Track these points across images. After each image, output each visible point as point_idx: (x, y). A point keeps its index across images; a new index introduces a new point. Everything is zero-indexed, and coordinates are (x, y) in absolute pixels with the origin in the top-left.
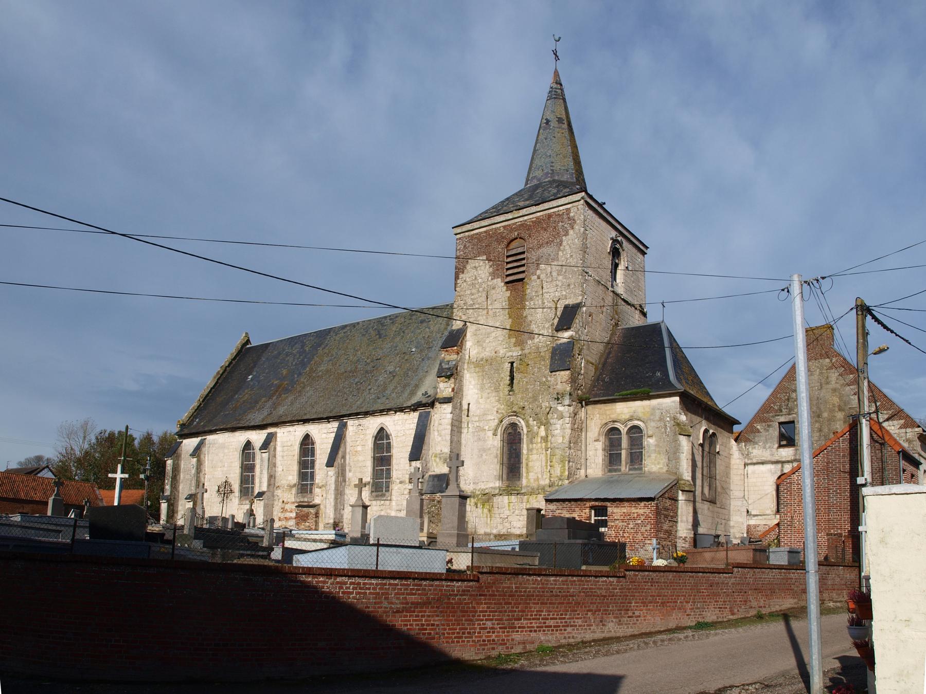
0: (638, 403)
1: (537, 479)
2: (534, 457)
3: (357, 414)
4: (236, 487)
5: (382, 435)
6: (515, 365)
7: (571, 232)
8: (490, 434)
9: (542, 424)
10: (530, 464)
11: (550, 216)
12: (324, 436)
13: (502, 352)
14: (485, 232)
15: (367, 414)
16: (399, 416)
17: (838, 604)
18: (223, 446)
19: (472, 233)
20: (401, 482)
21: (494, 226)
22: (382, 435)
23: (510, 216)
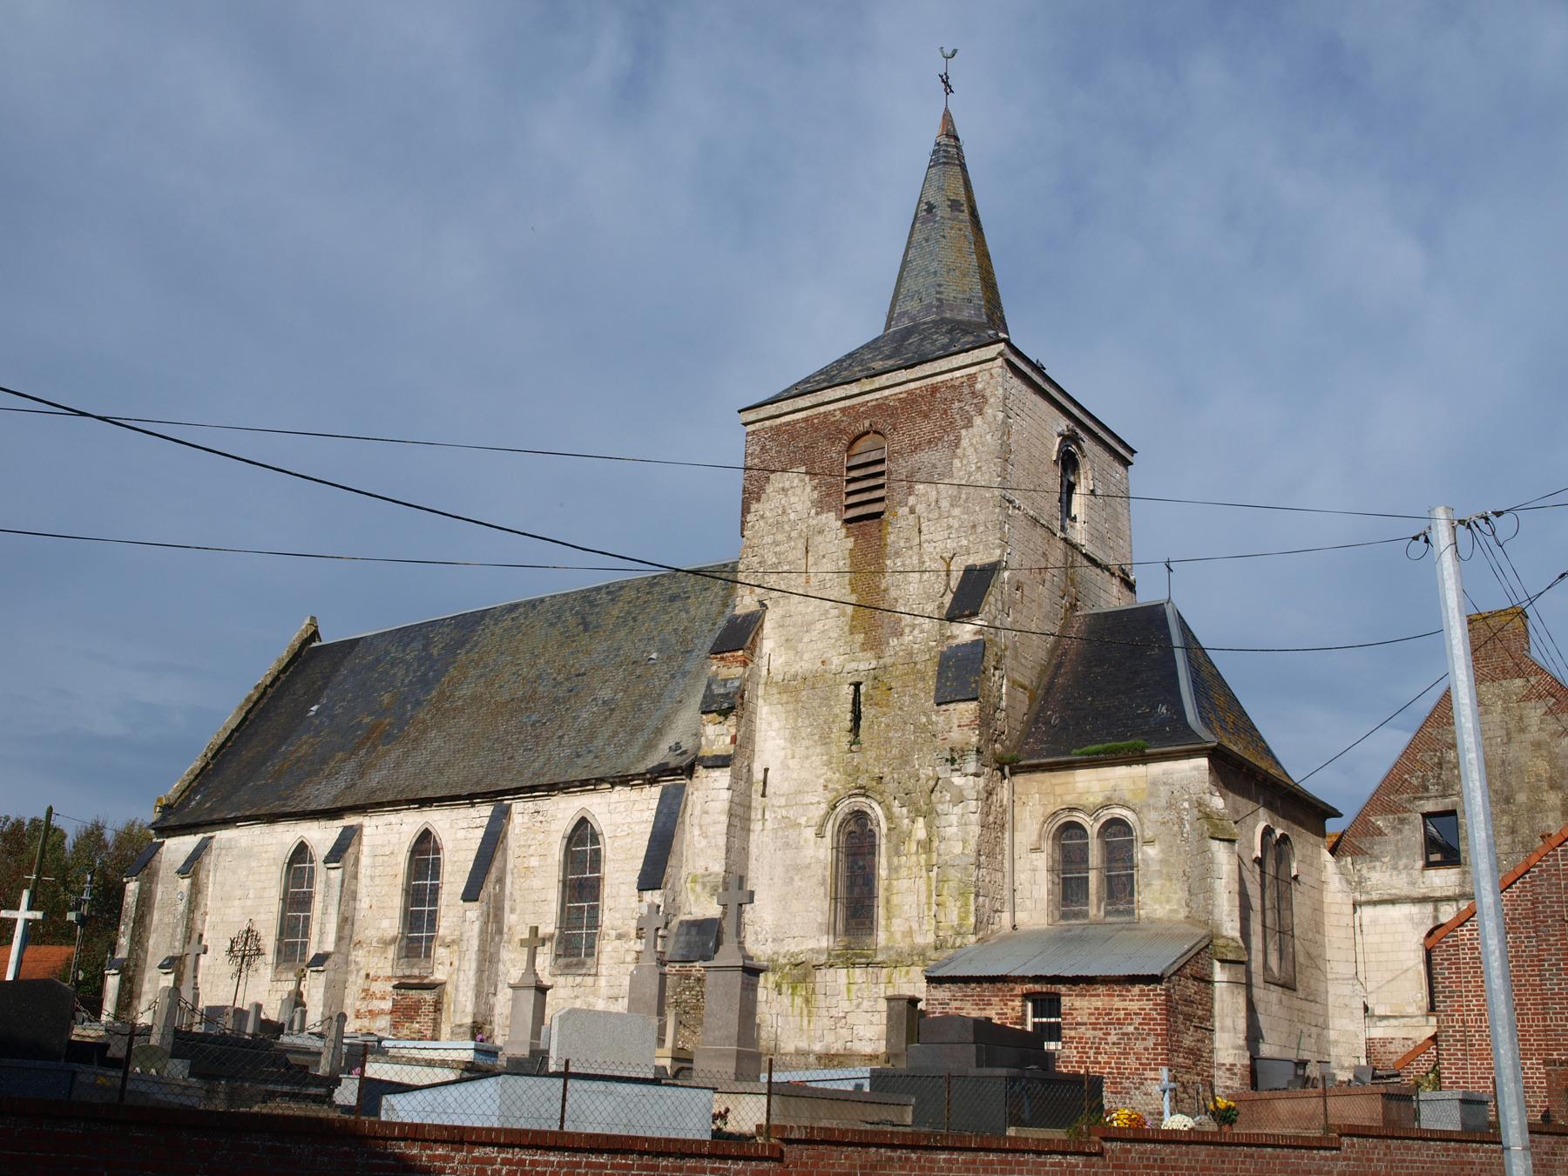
0: (1122, 771)
1: (910, 933)
2: (902, 884)
4: (269, 942)
6: (863, 689)
7: (978, 420)
8: (810, 833)
9: (918, 813)
10: (895, 900)
11: (934, 389)
12: (461, 834)
13: (836, 662)
14: (805, 420)
15: (553, 788)
16: (621, 794)
20: (619, 937)
23: (854, 389)
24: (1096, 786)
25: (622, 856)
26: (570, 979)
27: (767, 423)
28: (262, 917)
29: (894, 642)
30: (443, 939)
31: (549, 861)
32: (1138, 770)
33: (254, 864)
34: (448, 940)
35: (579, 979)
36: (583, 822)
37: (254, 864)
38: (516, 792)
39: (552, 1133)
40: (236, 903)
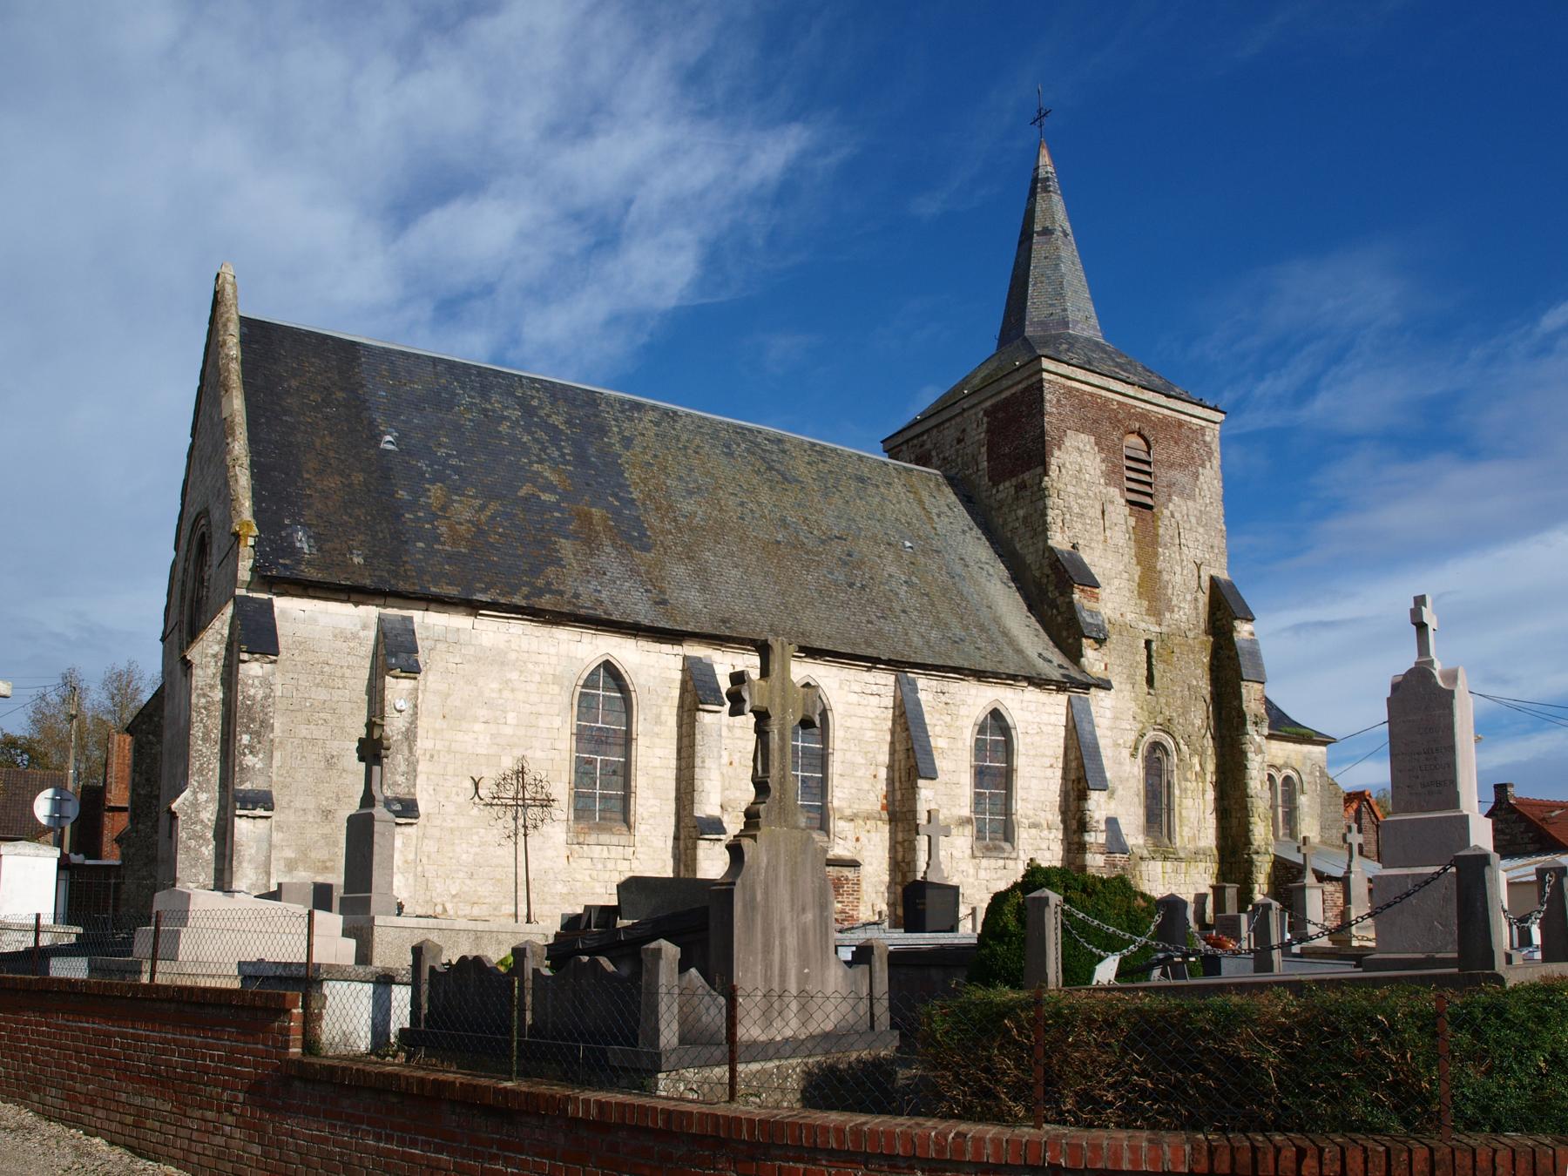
0: (1290, 746)
1: (1194, 838)
2: (1188, 802)
3: (1014, 677)
4: (561, 790)
5: (997, 721)
6: (1154, 646)
7: (1208, 465)
8: (1126, 753)
9: (1195, 751)
10: (1184, 813)
11: (1180, 424)
12: (854, 698)
13: (1129, 617)
14: (1091, 394)
15: (980, 675)
16: (1032, 694)
17: (198, 1113)
18: (498, 659)
19: (1069, 383)
20: (1035, 826)
21: (1104, 393)
22: (997, 721)
23: (1130, 390)
24: (1280, 753)
25: (1032, 753)
26: (992, 861)
27: (1063, 380)
28: (539, 754)
29: (1168, 615)
30: (840, 810)
31: (960, 745)
32: (1298, 747)
33: (514, 676)
34: (848, 812)
35: (1001, 862)
36: (996, 715)
37: (514, 676)
38: (925, 667)
39: (301, 965)
40: (478, 727)
